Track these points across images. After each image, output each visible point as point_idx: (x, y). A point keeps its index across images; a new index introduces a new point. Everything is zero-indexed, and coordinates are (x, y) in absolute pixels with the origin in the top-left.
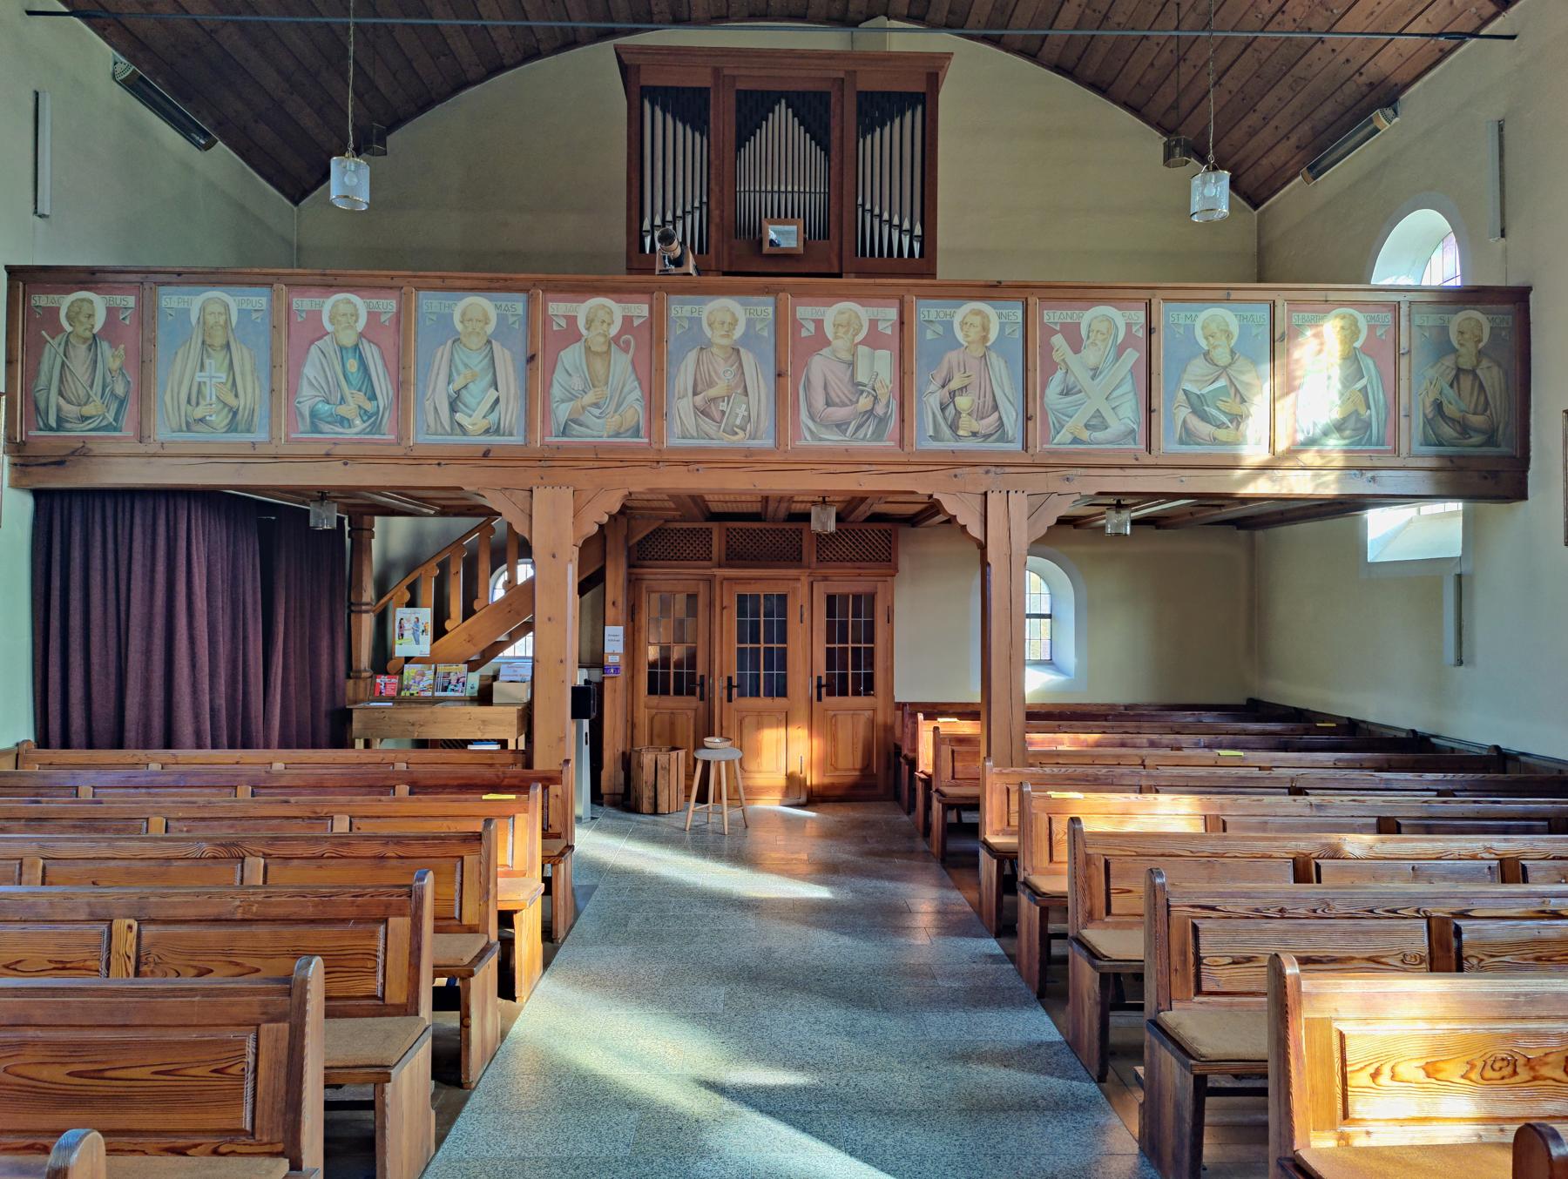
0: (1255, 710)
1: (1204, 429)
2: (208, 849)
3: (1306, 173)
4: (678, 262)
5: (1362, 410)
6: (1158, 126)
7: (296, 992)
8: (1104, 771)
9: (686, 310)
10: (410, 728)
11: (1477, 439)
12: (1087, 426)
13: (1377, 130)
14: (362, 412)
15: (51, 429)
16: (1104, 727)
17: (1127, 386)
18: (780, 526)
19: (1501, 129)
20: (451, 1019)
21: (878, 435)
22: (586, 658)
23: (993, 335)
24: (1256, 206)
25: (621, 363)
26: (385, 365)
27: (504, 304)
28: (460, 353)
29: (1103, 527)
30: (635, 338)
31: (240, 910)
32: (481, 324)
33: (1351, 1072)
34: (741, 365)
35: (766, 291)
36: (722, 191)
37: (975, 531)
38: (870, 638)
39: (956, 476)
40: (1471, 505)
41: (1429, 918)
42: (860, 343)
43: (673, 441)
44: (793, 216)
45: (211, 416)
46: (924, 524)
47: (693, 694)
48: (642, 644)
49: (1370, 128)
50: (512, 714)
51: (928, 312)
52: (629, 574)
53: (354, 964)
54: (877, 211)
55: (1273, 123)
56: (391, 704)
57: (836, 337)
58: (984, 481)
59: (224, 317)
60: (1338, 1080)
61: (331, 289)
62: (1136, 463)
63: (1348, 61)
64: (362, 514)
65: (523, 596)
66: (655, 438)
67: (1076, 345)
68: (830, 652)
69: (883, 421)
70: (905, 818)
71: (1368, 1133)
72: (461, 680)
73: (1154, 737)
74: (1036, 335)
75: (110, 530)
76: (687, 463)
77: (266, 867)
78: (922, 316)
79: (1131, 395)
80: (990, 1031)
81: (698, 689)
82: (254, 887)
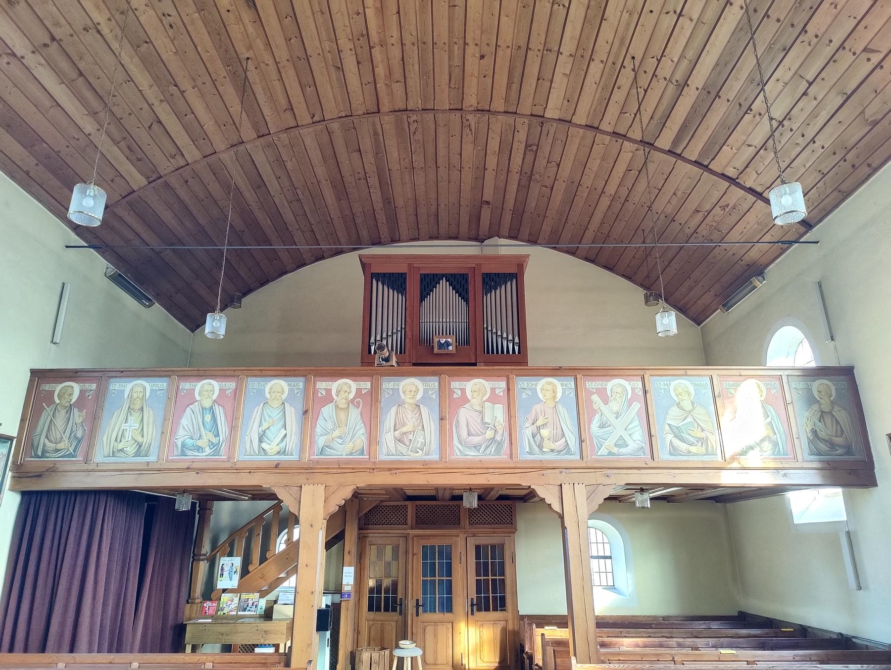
0: (743, 619)
1: (683, 446)
4: (387, 360)
5: (772, 435)
6: (642, 285)
8: (648, 666)
9: (391, 385)
10: (220, 637)
11: (840, 451)
12: (616, 445)
14: (210, 443)
15: (38, 457)
17: (636, 423)
19: (820, 286)
21: (498, 451)
22: (332, 587)
24: (699, 325)
25: (355, 414)
27: (293, 383)
28: (267, 409)
29: (634, 502)
30: (363, 401)
32: (280, 394)
35: (434, 374)
37: (556, 507)
38: (502, 573)
39: (543, 475)
40: (847, 489)
42: (486, 401)
45: (127, 448)
46: (530, 501)
48: (366, 578)
49: (752, 286)
50: (283, 627)
51: (522, 384)
52: (359, 534)
54: (494, 331)
55: (701, 284)
56: (210, 620)
57: (473, 398)
59: (142, 394)
61: (202, 378)
62: (646, 466)
64: (207, 500)
66: (372, 455)
67: (606, 401)
69: (500, 444)
72: (255, 604)
73: (680, 640)
74: (583, 395)
75: (60, 514)
76: (390, 470)
79: (639, 427)
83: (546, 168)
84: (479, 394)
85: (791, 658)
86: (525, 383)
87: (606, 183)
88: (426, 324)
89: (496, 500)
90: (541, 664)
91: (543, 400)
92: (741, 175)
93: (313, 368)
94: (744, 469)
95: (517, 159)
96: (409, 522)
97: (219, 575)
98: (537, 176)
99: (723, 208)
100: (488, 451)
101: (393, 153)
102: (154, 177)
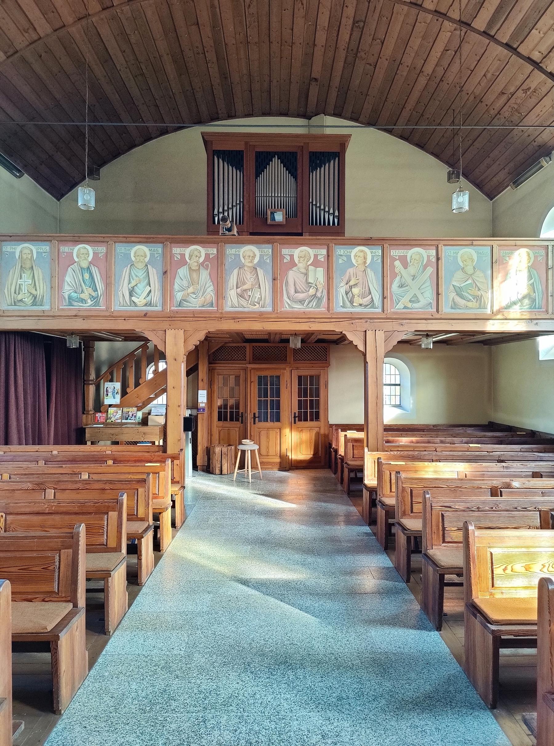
0: (492, 426)
2: (30, 486)
3: (512, 185)
4: (229, 230)
5: (532, 294)
6: (447, 163)
7: (75, 537)
9: (233, 251)
10: (111, 436)
12: (410, 301)
13: (542, 167)
14: (91, 296)
16: (422, 434)
17: (428, 284)
18: (277, 345)
20: (134, 559)
21: (318, 305)
22: (190, 405)
23: (368, 261)
24: (491, 199)
25: (205, 275)
26: (101, 276)
28: (134, 270)
29: (421, 345)
31: (48, 509)
33: (495, 568)
34: (257, 274)
35: (268, 242)
36: (249, 196)
37: (361, 348)
38: (318, 395)
39: (352, 324)
41: (540, 511)
42: (310, 265)
43: (228, 308)
44: (281, 208)
47: (239, 421)
48: (215, 399)
49: (539, 165)
50: (157, 431)
51: (340, 251)
52: (209, 367)
53: (94, 531)
54: (318, 205)
55: (498, 163)
57: (299, 262)
58: (365, 326)
59: (30, 255)
60: (490, 572)
61: (78, 243)
62: (432, 317)
63: (529, 136)
65: (162, 376)
66: (220, 307)
68: (300, 401)
69: (320, 299)
70: (333, 476)
71: (502, 593)
72: (134, 415)
74: (388, 261)
76: (234, 318)
77: (55, 493)
78: (337, 253)
79: (430, 287)
80: (363, 563)
81: (240, 418)
82: (51, 500)
83: (371, 46)
84: (304, 259)
85: (519, 450)
86: (342, 251)
87: (425, 62)
88: (260, 198)
89: (314, 342)
90: (343, 454)
91: (355, 264)
92: (544, 60)
93: (169, 236)
94: (506, 319)
95: (345, 35)
96: (248, 358)
97: (105, 395)
98: (362, 54)
99: (525, 91)
100: (310, 305)
101: (230, 27)
102: (11, 51)
